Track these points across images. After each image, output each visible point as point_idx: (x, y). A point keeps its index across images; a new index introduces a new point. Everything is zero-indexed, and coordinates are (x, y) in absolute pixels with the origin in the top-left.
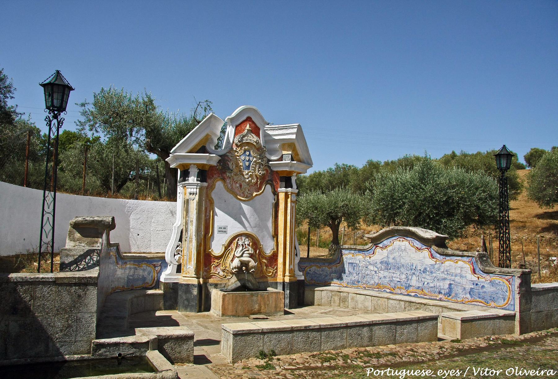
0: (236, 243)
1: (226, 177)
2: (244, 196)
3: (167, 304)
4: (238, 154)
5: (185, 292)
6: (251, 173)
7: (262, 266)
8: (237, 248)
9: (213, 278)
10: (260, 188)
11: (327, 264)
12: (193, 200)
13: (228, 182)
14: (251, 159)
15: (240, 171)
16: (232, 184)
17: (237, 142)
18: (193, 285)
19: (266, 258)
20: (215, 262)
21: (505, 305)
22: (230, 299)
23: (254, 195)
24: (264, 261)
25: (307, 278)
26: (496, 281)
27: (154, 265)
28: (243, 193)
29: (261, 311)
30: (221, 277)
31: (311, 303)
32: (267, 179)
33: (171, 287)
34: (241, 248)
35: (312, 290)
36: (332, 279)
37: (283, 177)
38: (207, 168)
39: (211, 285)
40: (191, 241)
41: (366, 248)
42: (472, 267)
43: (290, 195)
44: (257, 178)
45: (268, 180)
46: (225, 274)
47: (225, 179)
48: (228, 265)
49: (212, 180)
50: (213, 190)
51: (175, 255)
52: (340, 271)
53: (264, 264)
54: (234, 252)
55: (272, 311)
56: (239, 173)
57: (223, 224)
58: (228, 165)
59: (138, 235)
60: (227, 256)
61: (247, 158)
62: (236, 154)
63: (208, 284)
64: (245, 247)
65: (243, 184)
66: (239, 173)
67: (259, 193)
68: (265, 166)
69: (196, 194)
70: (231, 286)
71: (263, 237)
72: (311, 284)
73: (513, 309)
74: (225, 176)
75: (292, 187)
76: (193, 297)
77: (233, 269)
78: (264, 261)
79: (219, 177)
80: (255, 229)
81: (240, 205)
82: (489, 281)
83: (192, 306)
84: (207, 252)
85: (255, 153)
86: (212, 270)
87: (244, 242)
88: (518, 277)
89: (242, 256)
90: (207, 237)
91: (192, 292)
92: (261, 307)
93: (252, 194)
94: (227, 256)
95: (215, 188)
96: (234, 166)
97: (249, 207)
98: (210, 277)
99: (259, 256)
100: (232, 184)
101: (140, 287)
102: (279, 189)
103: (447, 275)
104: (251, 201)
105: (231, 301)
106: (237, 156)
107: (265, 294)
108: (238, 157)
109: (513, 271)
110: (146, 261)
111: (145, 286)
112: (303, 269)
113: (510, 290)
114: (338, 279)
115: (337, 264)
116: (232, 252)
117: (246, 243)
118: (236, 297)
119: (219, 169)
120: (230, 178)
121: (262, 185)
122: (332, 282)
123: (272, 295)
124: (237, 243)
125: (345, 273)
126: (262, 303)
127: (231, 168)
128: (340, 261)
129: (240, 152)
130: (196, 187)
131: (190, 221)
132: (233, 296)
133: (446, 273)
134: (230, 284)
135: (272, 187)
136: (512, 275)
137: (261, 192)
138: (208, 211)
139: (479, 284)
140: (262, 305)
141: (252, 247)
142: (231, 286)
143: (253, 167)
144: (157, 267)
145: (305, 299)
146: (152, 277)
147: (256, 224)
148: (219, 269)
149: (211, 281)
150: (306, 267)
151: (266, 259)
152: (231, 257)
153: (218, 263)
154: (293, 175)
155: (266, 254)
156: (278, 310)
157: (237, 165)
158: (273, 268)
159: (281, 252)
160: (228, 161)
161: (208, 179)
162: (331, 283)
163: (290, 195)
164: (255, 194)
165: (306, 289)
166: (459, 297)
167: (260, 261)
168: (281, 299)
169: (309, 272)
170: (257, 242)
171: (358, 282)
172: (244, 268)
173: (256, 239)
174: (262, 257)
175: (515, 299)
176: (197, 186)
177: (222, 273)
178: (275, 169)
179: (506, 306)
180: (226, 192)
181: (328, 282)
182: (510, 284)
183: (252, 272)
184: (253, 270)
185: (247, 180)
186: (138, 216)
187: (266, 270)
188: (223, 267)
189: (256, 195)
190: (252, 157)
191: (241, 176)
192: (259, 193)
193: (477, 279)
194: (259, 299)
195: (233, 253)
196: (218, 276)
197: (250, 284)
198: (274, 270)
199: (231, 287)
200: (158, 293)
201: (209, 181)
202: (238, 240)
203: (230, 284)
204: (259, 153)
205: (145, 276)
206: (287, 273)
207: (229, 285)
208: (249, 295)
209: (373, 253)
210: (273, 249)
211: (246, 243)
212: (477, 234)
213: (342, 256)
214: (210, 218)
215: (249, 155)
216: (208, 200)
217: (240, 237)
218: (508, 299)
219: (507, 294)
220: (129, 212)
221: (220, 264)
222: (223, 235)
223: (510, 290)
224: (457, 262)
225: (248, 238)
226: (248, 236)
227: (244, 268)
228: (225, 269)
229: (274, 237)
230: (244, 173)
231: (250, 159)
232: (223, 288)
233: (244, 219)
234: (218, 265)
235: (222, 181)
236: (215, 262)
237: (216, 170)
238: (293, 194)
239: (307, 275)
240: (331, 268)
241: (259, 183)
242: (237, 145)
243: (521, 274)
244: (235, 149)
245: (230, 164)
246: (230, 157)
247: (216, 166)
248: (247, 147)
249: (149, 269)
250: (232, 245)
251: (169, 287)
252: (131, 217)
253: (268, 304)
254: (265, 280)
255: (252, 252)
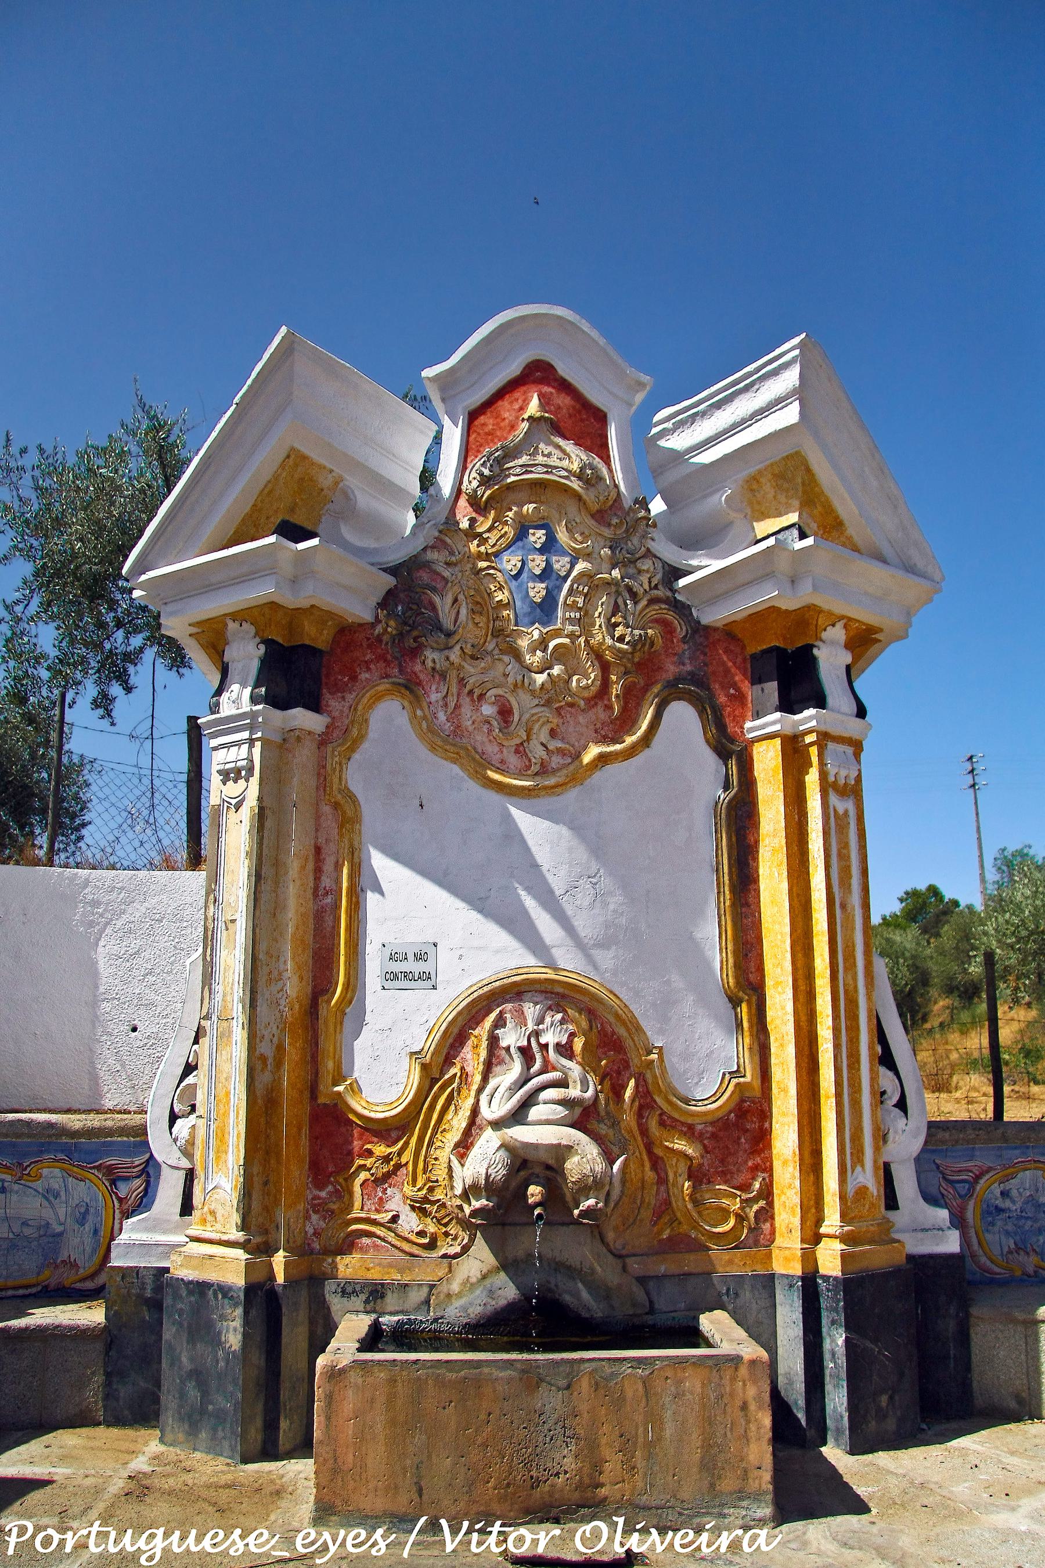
0: (484, 1044)
1: (422, 676)
2: (529, 767)
3: (124, 1391)
4: (482, 549)
5: (190, 1326)
6: (567, 641)
7: (662, 1180)
8: (497, 1069)
9: (364, 1250)
10: (626, 722)
12: (238, 807)
13: (434, 697)
14: (560, 564)
15: (499, 633)
16: (457, 707)
17: (475, 484)
18: (224, 1290)
19: (691, 1127)
20: (370, 1153)
22: (372, 1401)
23: (587, 758)
24: (680, 1145)
25: (988, 1236)
27: (110, 1170)
28: (520, 750)
29: (603, 1491)
30: (406, 1247)
31: (1020, 1401)
32: (671, 669)
33: (148, 1294)
34: (516, 1068)
35: (1019, 1315)
37: (764, 652)
38: (317, 636)
39: (347, 1291)
40: (225, 1036)
43: (814, 751)
44: (605, 668)
45: (678, 679)
46: (432, 1228)
47: (419, 684)
48: (440, 1173)
49: (350, 697)
50: (352, 749)
51: (173, 1118)
53: (683, 1168)
54: (473, 1093)
55: (685, 1494)
56: (490, 646)
57: (412, 937)
58: (433, 608)
59: (134, 1029)
60: (435, 1116)
61: (537, 564)
62: (473, 546)
63: (330, 1286)
64: (546, 1061)
65: (522, 704)
66: (490, 646)
67: (618, 747)
68: (652, 601)
69: (250, 770)
70: (462, 1302)
71: (666, 1004)
72: (1018, 1273)
74: (418, 668)
75: (820, 702)
76: (222, 1364)
77: (465, 1196)
78: (680, 1145)
79: (387, 676)
80: (606, 959)
81: (508, 818)
83: (220, 1416)
84: (322, 1100)
85: (586, 538)
86: (357, 1204)
87: (537, 1034)
89: (518, 1116)
90: (323, 1011)
91: (220, 1333)
92: (597, 1466)
93: (577, 756)
94: (435, 1116)
95: (361, 737)
96: (464, 611)
97: (564, 831)
98: (347, 1246)
99: (640, 1115)
100: (457, 707)
101: (26, 1287)
102: (748, 725)
104: (572, 795)
105: (378, 1419)
106: (480, 556)
107: (626, 1369)
108: (483, 564)
110: (68, 1150)
111: (53, 1282)
112: (963, 1188)
116: (464, 1092)
117: (550, 1038)
118: (419, 1385)
119: (385, 638)
120: (443, 676)
121: (639, 705)
123: (679, 1382)
124: (493, 1041)
126: (607, 1437)
127: (447, 621)
129: (493, 537)
130: (245, 735)
131: (221, 925)
132: (392, 1381)
134: (455, 1287)
135: (701, 712)
137: (630, 740)
138: (328, 867)
140: (606, 1452)
141: (589, 1063)
142: (462, 1302)
143: (574, 606)
144: (126, 1179)
145: (975, 1375)
146: (96, 1232)
147: (607, 926)
148: (398, 1197)
149: (348, 1266)
150: (978, 1178)
151: (690, 1132)
152: (458, 1122)
153: (387, 1159)
154: (824, 635)
155: (687, 1101)
156: (728, 1484)
157: (482, 604)
158: (745, 1187)
159: (785, 1090)
160: (434, 590)
161: (328, 696)
163: (814, 751)
164: (593, 751)
165: (974, 1311)
167: (649, 1147)
168: (744, 1407)
169: (999, 1202)
170: (622, 1031)
172: (535, 1192)
173: (617, 1016)
174: (662, 1124)
176: (252, 728)
177: (410, 1222)
178: (714, 615)
180: (423, 751)
183: (584, 1214)
184: (591, 1202)
185: (540, 678)
186: (135, 944)
187: (696, 1202)
188: (419, 1184)
189: (603, 759)
190: (564, 553)
191: (506, 659)
192: (618, 747)
194: (584, 1407)
195: (471, 1101)
196: (391, 1237)
197: (585, 1295)
198: (748, 1202)
199: (464, 1309)
200: (71, 1328)
201: (334, 704)
202: (500, 1022)
203: (455, 1287)
204: (607, 532)
205: (59, 1229)
206: (832, 1221)
207: (449, 1296)
208: (510, 1380)
210: (737, 1073)
211: (550, 1038)
214: (337, 906)
215: (550, 546)
216: (326, 809)
217: (509, 1006)
220: (91, 924)
221: (398, 1166)
222: (414, 998)
225: (558, 1008)
226: (563, 996)
227: (535, 1192)
228: (425, 1200)
229: (735, 1002)
230: (523, 643)
231: (556, 566)
232: (417, 1309)
233: (530, 903)
234: (387, 1176)
235: (403, 696)
236: (370, 1153)
237: (369, 646)
238: (831, 746)
239: (992, 1224)
241: (616, 689)
242: (474, 501)
244: (464, 524)
245: (443, 605)
246: (440, 569)
247: (373, 625)
248: (532, 506)
249: (80, 1191)
250: (467, 1052)
251: (140, 1296)
252: (100, 949)
253: (649, 1445)
254: (690, 1262)
255: (590, 1093)
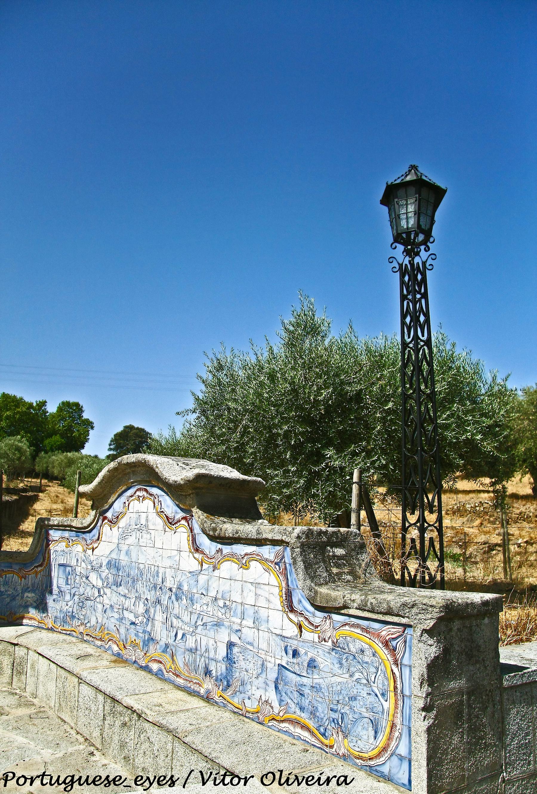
11: (17, 567)
21: (379, 755)
26: (351, 646)
36: (26, 607)
41: (85, 525)
42: (284, 584)
52: (42, 585)
73: (406, 782)
82: (330, 643)
88: (425, 631)
103: (223, 611)
109: (404, 605)
113: (395, 688)
114: (37, 608)
115: (37, 567)
122: (26, 615)
125: (51, 593)
128: (44, 560)
133: (221, 603)
136: (404, 621)
139: (302, 651)
162: (23, 618)
166: (249, 693)
171: (73, 617)
175: (413, 733)
179: (382, 760)
181: (18, 615)
182: (396, 663)
193: (296, 630)
209: (98, 539)
212: (523, 517)
213: (48, 545)
218: (388, 729)
219: (386, 705)
223: (395, 688)
224: (245, 566)
240: (25, 579)
243: (440, 619)
